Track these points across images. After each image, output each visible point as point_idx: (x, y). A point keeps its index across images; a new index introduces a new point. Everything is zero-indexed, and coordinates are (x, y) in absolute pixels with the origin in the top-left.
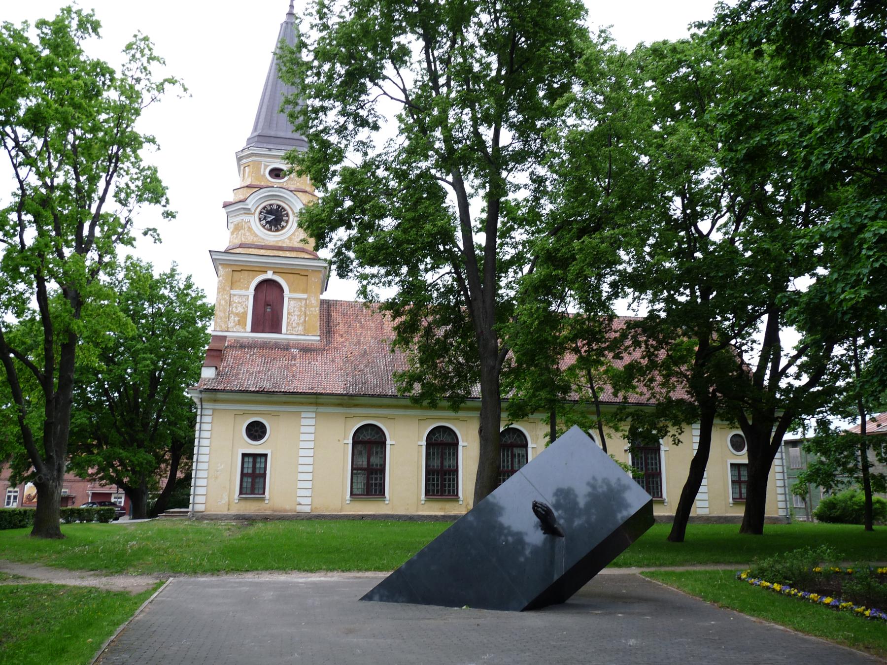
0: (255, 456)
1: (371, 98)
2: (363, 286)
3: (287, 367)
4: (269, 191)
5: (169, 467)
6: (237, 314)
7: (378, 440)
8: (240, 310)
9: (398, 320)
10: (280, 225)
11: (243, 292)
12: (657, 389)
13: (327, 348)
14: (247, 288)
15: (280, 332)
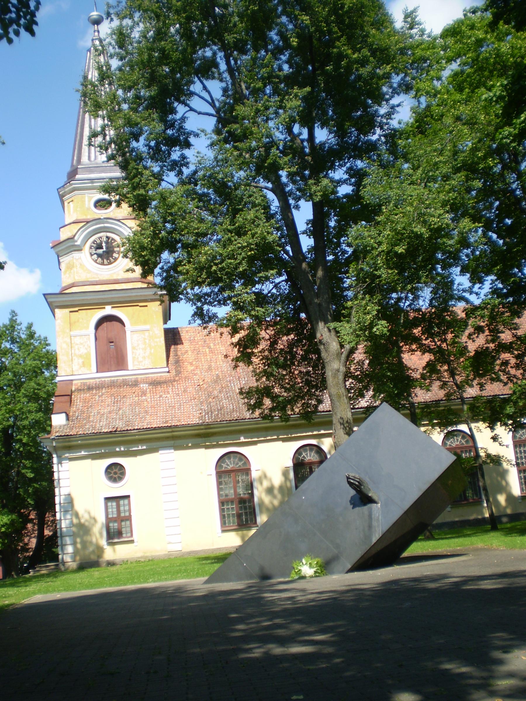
0: (117, 499)
1: (178, 116)
2: (197, 308)
3: (138, 404)
4: (96, 224)
5: (36, 527)
6: (81, 356)
7: (242, 467)
8: (83, 351)
9: (237, 337)
10: (112, 256)
11: (83, 332)
12: (513, 371)
13: (177, 378)
14: (87, 327)
15: (126, 369)
